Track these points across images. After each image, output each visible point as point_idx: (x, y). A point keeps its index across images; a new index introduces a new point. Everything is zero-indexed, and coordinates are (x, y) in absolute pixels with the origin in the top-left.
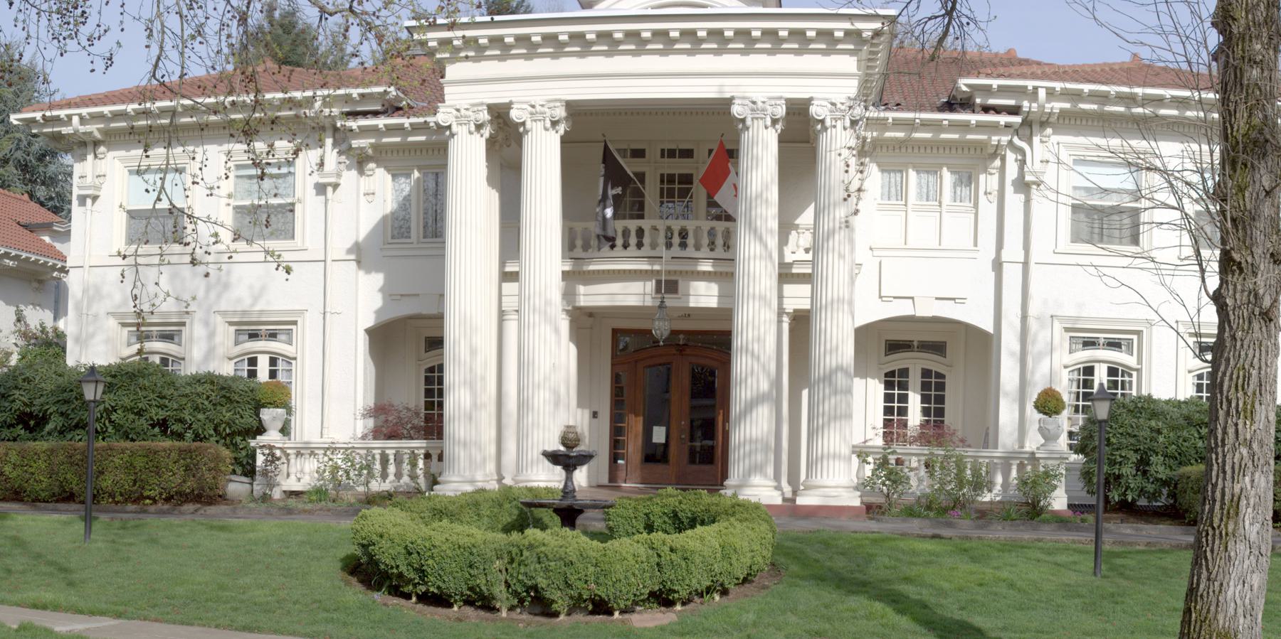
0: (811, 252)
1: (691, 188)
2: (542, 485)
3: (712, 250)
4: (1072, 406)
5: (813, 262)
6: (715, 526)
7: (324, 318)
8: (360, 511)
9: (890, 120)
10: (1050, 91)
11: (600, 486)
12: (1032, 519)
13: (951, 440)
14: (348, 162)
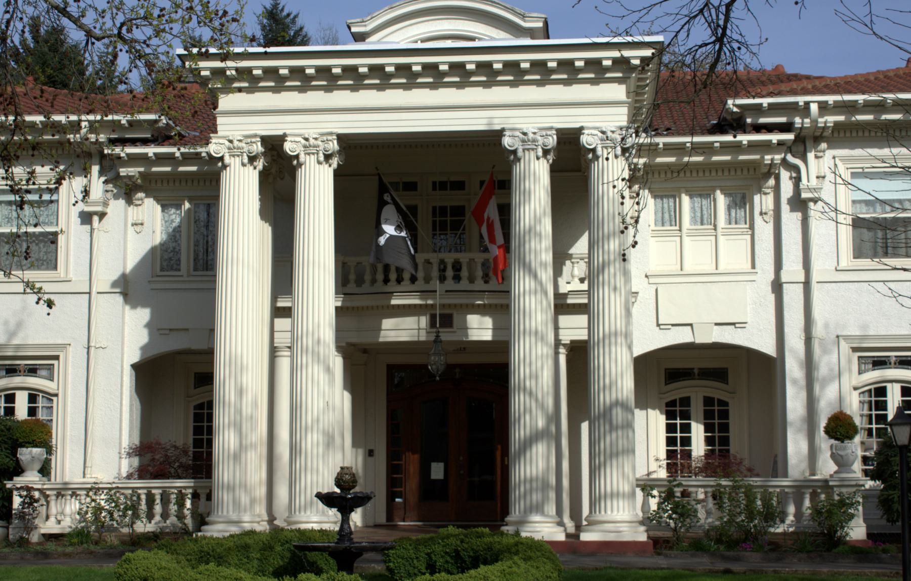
0: (586, 282)
1: (464, 220)
2: (316, 527)
3: (486, 282)
4: (865, 429)
5: (589, 292)
6: (498, 566)
7: (88, 353)
8: (124, 554)
9: (661, 146)
10: (823, 105)
11: (377, 526)
12: (829, 550)
13: (738, 470)
14: (115, 191)
